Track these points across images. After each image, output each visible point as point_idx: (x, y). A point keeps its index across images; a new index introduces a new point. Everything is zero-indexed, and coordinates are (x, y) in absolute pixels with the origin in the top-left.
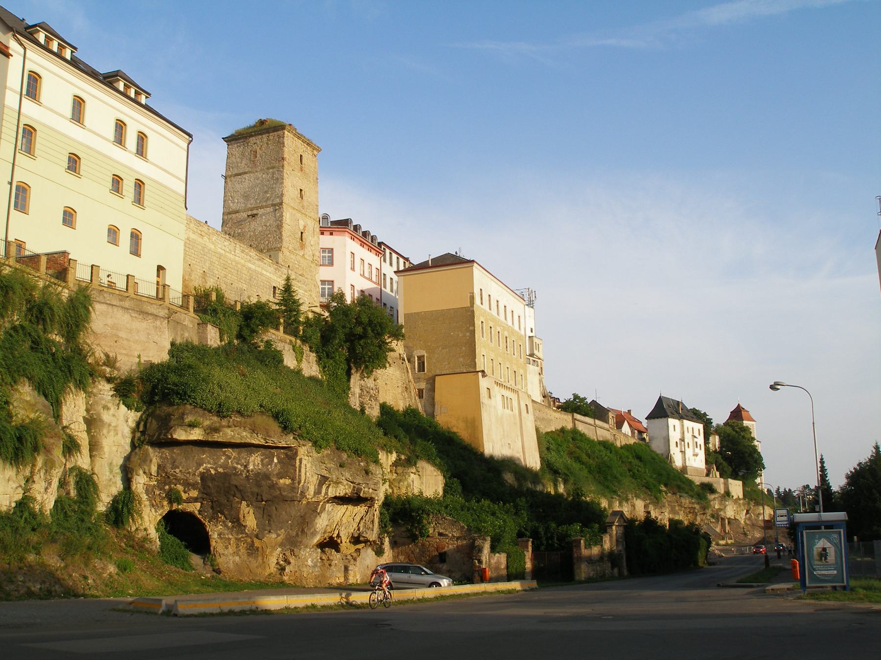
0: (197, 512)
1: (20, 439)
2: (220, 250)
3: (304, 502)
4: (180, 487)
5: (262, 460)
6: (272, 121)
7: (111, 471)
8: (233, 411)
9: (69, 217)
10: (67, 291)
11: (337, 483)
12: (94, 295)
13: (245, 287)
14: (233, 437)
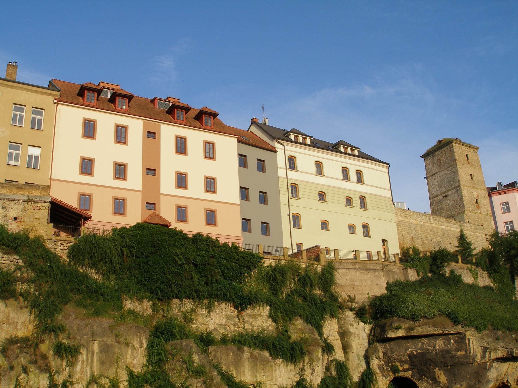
0: (410, 377)
1: (293, 349)
2: (420, 223)
3: (476, 364)
4: (398, 364)
5: (444, 343)
6: (445, 139)
7: (359, 359)
8: (421, 317)
9: (325, 225)
10: (320, 266)
11: (496, 350)
12: (336, 265)
13: (440, 240)
14: (422, 331)
